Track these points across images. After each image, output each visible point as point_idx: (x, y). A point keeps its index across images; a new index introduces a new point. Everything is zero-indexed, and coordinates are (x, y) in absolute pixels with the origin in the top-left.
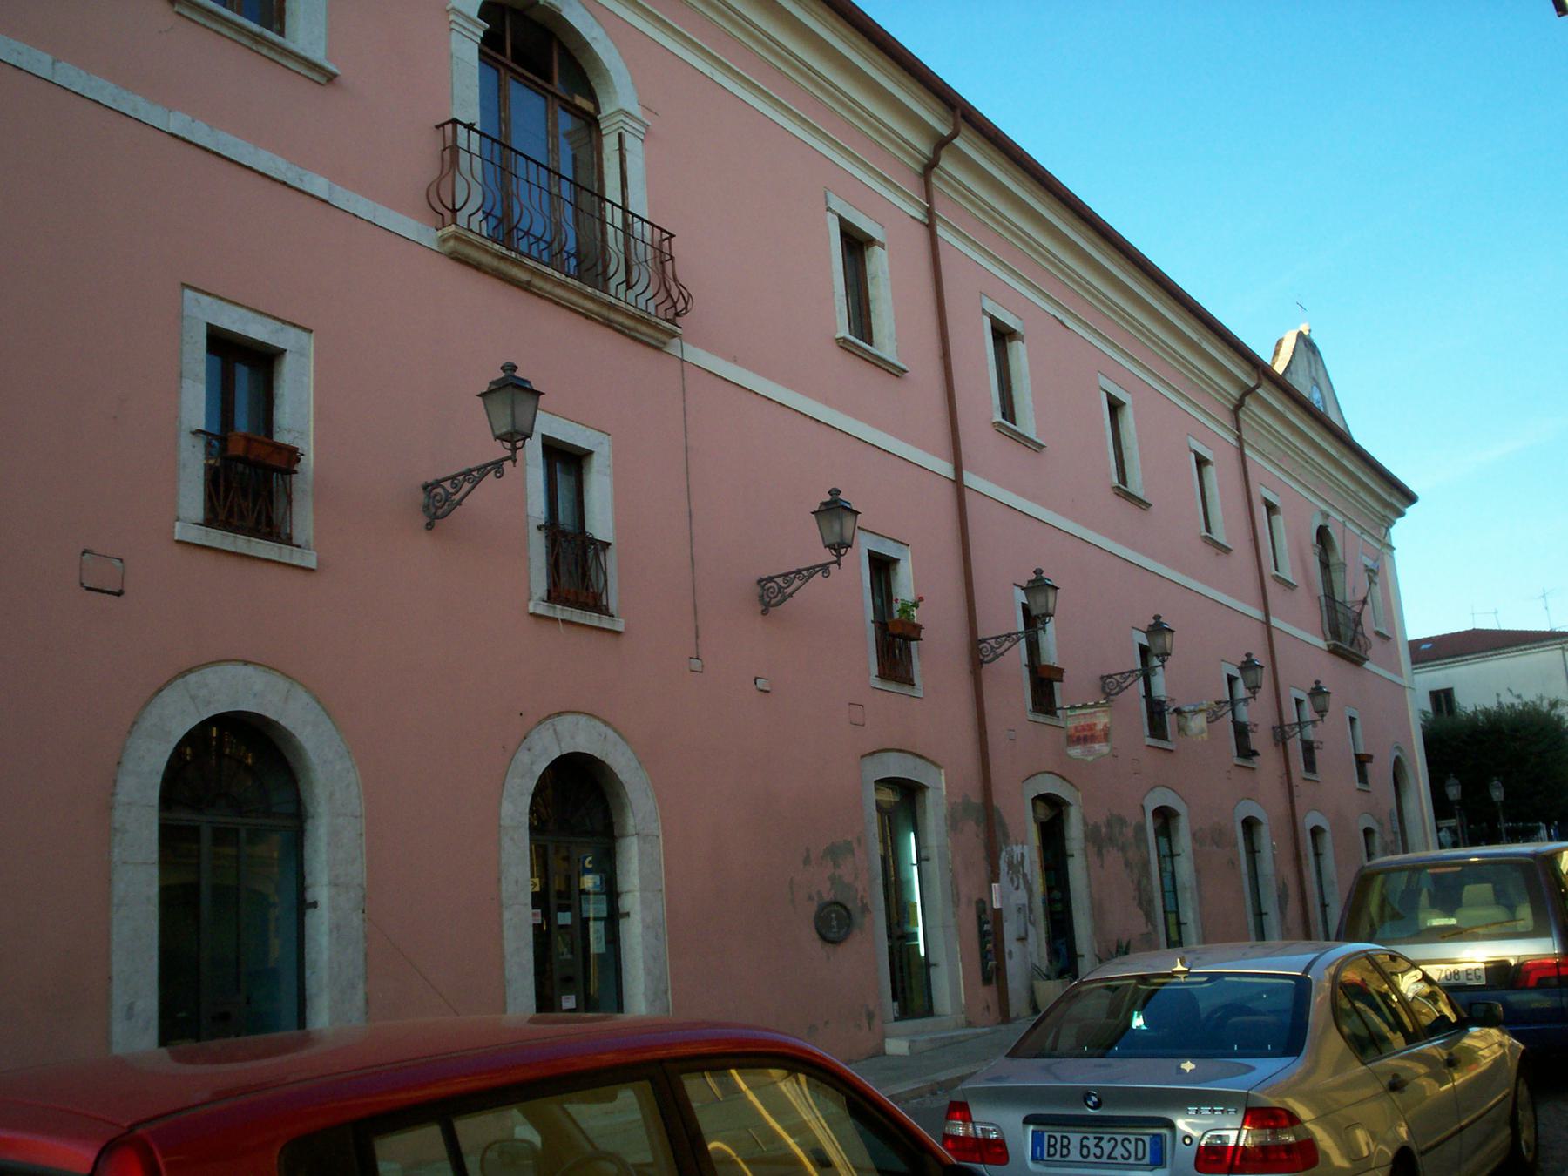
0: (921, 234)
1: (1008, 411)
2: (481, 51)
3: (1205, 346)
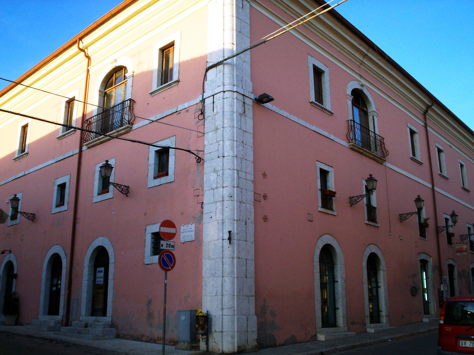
0: (423, 129)
1: (414, 154)
2: (352, 103)
3: (370, 55)
